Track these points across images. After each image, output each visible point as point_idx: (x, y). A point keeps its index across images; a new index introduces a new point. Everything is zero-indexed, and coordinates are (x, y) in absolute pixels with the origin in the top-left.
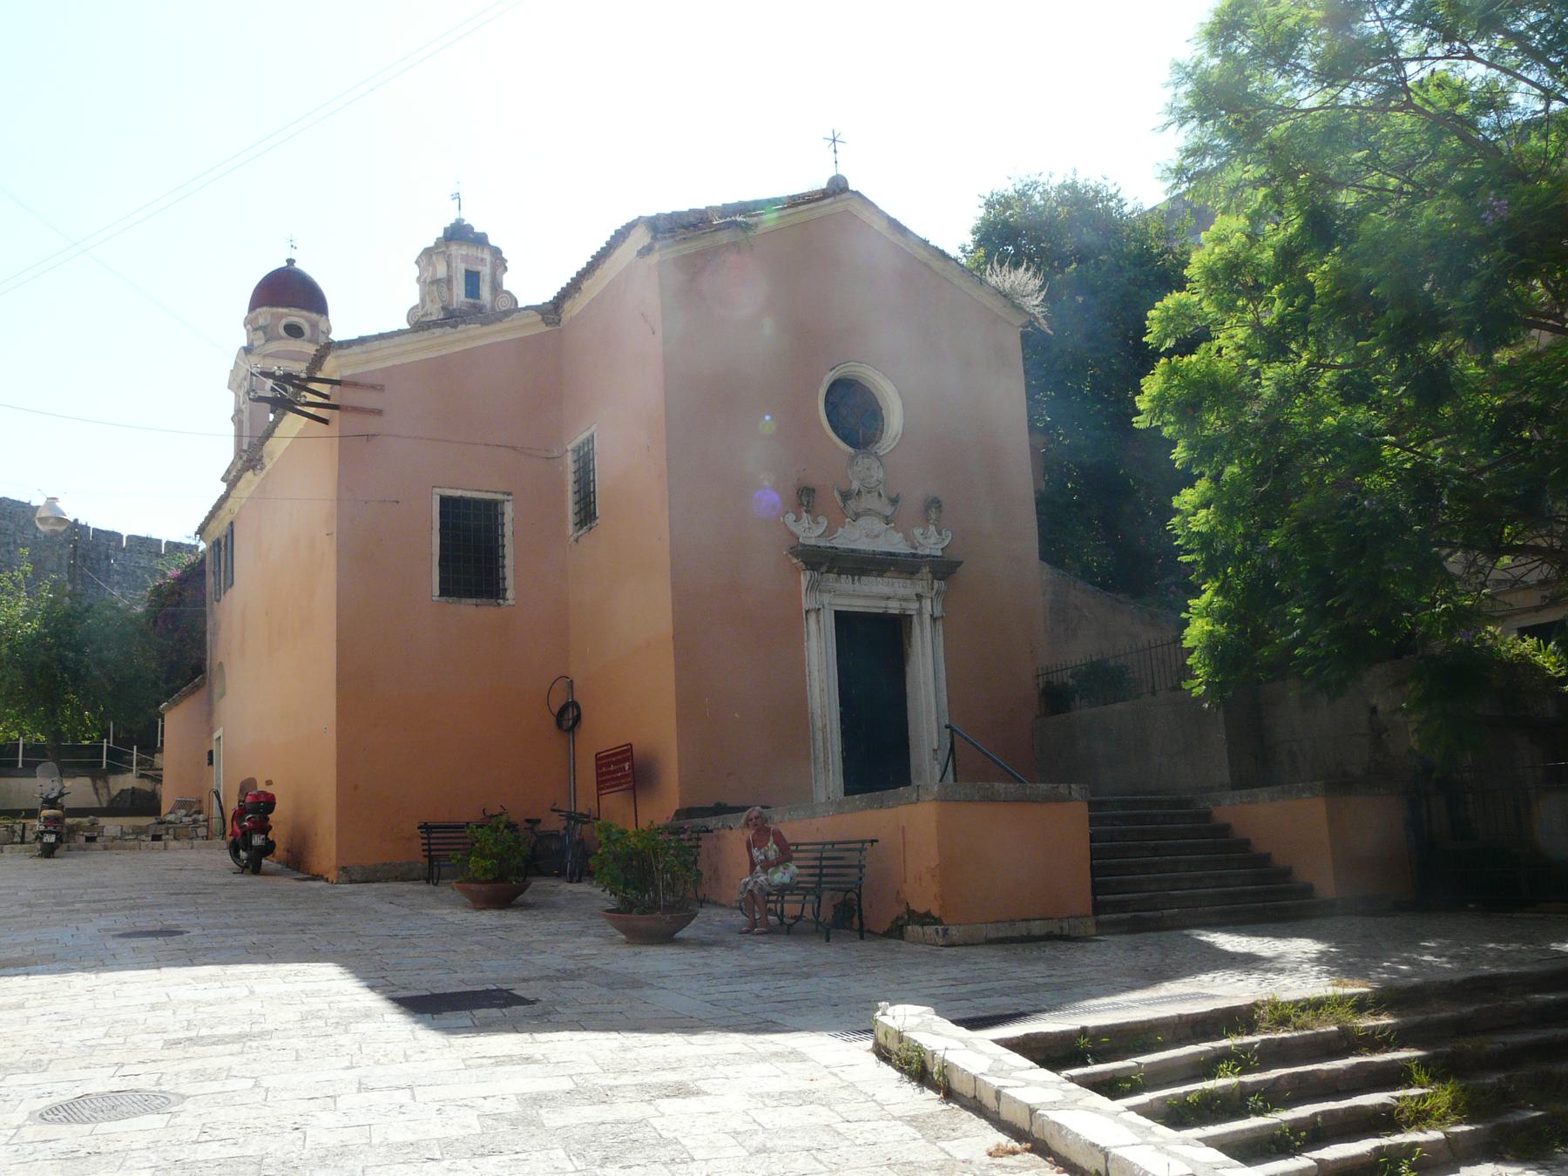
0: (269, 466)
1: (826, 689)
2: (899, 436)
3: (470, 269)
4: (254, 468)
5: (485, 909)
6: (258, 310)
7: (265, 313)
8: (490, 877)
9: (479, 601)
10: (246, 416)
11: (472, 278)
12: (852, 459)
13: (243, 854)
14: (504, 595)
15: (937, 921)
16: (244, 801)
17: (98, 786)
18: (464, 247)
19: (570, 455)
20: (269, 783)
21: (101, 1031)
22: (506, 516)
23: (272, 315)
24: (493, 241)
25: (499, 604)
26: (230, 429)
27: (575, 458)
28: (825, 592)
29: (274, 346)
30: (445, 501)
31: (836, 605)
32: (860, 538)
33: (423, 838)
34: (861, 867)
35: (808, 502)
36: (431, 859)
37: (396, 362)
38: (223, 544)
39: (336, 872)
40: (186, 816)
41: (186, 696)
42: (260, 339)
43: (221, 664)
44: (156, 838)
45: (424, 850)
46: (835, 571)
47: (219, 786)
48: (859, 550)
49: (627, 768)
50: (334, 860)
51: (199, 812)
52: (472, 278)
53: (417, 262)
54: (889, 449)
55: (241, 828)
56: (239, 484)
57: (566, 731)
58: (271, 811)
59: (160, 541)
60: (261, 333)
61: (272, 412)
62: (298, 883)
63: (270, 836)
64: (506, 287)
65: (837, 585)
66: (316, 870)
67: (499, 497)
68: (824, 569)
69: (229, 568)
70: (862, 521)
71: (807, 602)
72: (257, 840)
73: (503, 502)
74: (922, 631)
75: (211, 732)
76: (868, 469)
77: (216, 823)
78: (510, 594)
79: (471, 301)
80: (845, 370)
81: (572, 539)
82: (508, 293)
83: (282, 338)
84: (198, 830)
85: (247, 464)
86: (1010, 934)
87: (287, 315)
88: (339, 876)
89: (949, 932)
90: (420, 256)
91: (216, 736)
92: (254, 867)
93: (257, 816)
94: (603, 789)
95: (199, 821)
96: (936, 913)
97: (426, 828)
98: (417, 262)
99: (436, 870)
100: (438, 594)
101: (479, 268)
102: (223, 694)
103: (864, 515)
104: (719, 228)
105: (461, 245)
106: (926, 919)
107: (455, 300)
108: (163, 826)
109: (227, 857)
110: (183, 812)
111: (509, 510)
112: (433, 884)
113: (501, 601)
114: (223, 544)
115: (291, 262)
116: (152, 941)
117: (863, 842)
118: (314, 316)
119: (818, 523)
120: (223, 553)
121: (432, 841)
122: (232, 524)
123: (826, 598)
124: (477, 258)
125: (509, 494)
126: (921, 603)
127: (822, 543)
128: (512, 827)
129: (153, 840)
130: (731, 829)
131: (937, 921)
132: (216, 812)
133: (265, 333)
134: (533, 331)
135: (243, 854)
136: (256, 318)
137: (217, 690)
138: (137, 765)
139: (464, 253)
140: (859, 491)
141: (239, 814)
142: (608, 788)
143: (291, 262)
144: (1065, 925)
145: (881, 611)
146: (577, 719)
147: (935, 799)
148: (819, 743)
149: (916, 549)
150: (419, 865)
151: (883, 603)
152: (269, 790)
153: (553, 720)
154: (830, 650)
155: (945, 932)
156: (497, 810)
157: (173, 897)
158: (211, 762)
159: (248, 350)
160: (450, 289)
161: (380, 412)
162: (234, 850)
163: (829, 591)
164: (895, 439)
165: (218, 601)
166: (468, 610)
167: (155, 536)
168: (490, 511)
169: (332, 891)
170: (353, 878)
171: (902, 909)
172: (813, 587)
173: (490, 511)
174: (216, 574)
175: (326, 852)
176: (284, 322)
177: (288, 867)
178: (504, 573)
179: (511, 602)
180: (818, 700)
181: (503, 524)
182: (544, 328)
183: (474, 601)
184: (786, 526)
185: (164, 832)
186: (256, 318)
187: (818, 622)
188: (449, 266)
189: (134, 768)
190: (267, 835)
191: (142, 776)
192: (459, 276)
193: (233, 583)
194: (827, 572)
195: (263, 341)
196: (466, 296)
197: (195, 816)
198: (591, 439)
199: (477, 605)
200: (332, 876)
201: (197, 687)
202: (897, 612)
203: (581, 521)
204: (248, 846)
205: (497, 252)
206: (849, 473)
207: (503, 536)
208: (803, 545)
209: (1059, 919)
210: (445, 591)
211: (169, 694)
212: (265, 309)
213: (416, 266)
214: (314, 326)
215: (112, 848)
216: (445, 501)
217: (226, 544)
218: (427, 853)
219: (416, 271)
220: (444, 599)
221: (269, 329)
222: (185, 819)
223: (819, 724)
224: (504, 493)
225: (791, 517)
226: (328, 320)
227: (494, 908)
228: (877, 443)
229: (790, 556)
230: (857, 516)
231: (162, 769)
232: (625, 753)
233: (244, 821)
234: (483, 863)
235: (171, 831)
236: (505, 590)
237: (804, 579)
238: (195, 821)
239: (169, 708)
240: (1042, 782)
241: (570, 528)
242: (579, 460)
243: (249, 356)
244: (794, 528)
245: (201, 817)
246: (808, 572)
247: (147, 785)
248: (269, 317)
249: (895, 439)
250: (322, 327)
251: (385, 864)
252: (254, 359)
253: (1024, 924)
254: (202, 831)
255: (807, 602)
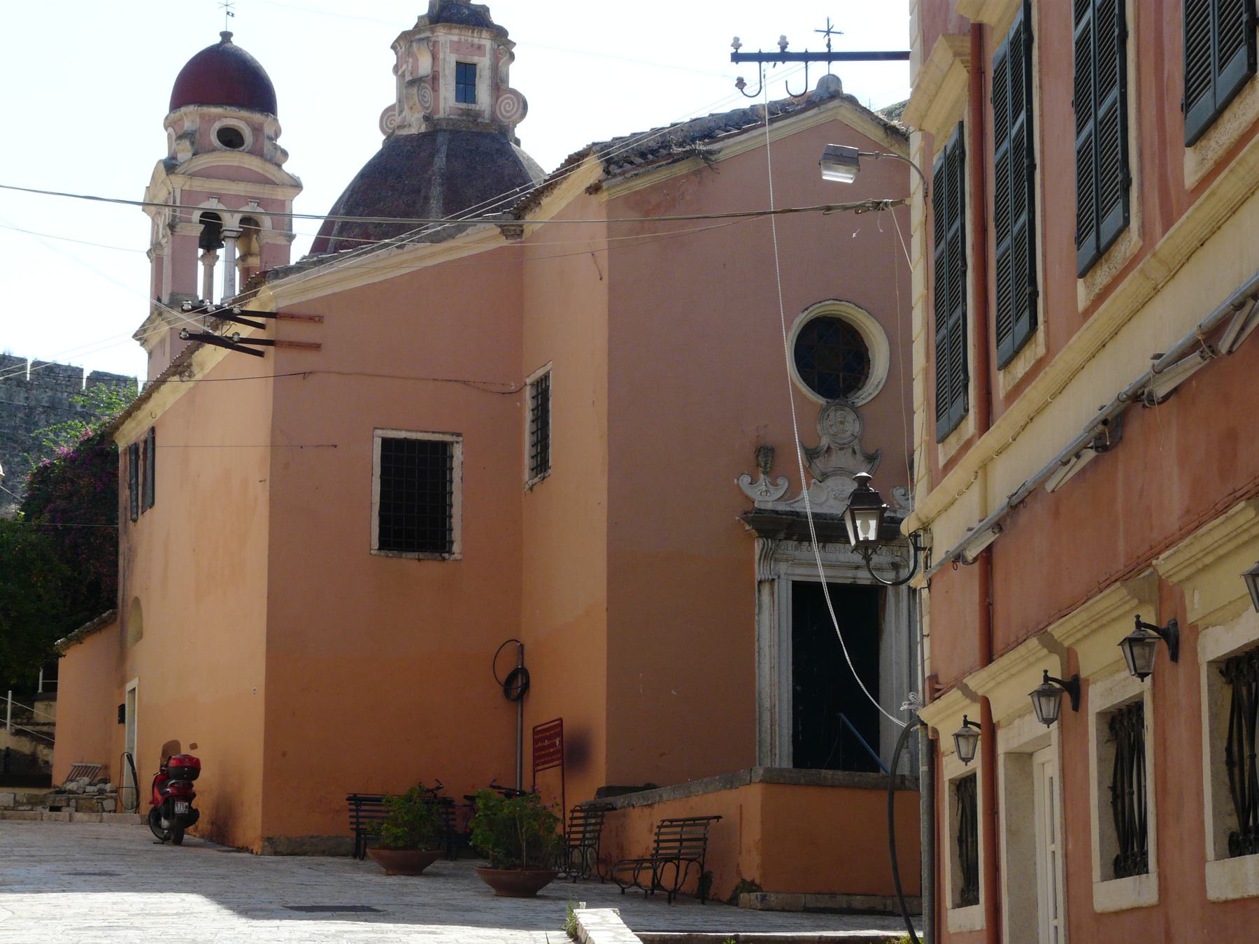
0: (199, 376)
1: (776, 667)
2: (883, 382)
3: (462, 60)
4: (181, 374)
5: (395, 875)
6: (183, 110)
7: (192, 115)
8: (401, 843)
9: (421, 556)
10: (167, 251)
11: (466, 74)
12: (824, 410)
13: (165, 823)
14: (451, 547)
15: (758, 888)
16: (166, 766)
17: (1041, 701)
18: (456, 31)
19: (528, 388)
20: (194, 746)
21: (87, 910)
22: (455, 459)
23: (202, 117)
24: (496, 18)
25: (444, 559)
26: (146, 267)
27: (534, 393)
28: (781, 561)
29: (204, 161)
30: (386, 443)
31: (793, 575)
32: (827, 500)
33: (351, 810)
34: (705, 840)
35: (766, 464)
36: (359, 832)
37: (337, 289)
38: (141, 450)
39: (261, 843)
40: (90, 784)
41: (89, 632)
42: (185, 154)
43: (137, 600)
44: (54, 809)
45: (351, 823)
46: (795, 537)
47: (133, 749)
48: (826, 514)
49: (558, 743)
50: (260, 830)
51: (105, 781)
52: (466, 74)
53: (393, 47)
54: (871, 398)
55: (162, 794)
56: (163, 387)
57: (513, 700)
58: (196, 776)
59: (24, 360)
60: (186, 144)
61: (201, 246)
62: (219, 853)
63: (194, 805)
64: (513, 84)
65: (797, 553)
66: (240, 843)
67: (448, 438)
68: (782, 535)
69: (149, 479)
70: (830, 482)
71: (760, 572)
72: (180, 808)
73: (452, 443)
74: (897, 602)
75: (123, 681)
76: (842, 423)
77: (127, 794)
78: (456, 548)
79: (463, 106)
80: (822, 309)
81: (527, 487)
82: (514, 92)
83: (214, 150)
84: (105, 803)
85: (173, 369)
86: (829, 905)
87: (220, 117)
88: (263, 847)
89: (767, 898)
90: (397, 41)
91: (129, 687)
92: (175, 837)
93: (181, 782)
94: (538, 765)
95: (106, 791)
96: (757, 881)
97: (356, 800)
98: (393, 47)
99: (363, 842)
100: (377, 547)
101: (475, 59)
102: (140, 635)
103: (832, 475)
104: (676, 160)
105: (450, 28)
106: (751, 887)
107: (442, 105)
108: (64, 797)
109: (147, 832)
110: (86, 780)
111: (458, 452)
112: (360, 859)
113: (446, 555)
114: (141, 450)
115: (226, 36)
116: (98, 878)
117: (709, 819)
118: (257, 117)
119: (777, 485)
120: (141, 462)
121: (361, 814)
122: (153, 430)
123: (783, 568)
124: (472, 45)
125: (459, 435)
126: (897, 573)
127: (782, 507)
128: (448, 803)
129: (50, 811)
130: (634, 807)
131: (758, 888)
132: (127, 780)
133: (192, 143)
134: (493, 245)
135: (165, 823)
136: (181, 119)
137: (131, 631)
138: (12, 718)
139: (455, 38)
140: (829, 448)
141: (160, 782)
142: (543, 764)
143: (226, 36)
144: (889, 902)
145: (849, 581)
146: (526, 686)
147: (761, 781)
148: (767, 724)
149: (895, 512)
150: (348, 840)
151: (850, 573)
152: (194, 754)
153: (499, 690)
154: (784, 624)
155: (764, 898)
156: (432, 785)
157: (101, 856)
158: (122, 720)
159: (170, 166)
160: (435, 89)
161: (316, 347)
162: (153, 820)
163: (787, 561)
164: (877, 386)
165: (135, 521)
166: (410, 565)
167: (17, 353)
168: (437, 453)
169: (255, 860)
170: (279, 849)
171: (737, 880)
172: (767, 556)
173: (437, 453)
174: (133, 487)
175: (251, 824)
176: (217, 125)
177: (211, 840)
178: (450, 523)
179: (457, 556)
180: (768, 677)
181: (451, 469)
182: (504, 242)
183: (415, 555)
184: (740, 489)
185: (64, 804)
186: (181, 119)
187: (772, 594)
188: (434, 57)
189: (8, 721)
190: (190, 804)
191: (18, 733)
192: (447, 72)
193: (153, 503)
194: (786, 539)
195: (190, 154)
196: (457, 100)
197: (101, 786)
198: (546, 378)
199: (419, 560)
200: (257, 847)
201: (104, 624)
202: (868, 582)
203: (537, 467)
204: (170, 814)
205: (500, 34)
206: (819, 427)
207: (451, 482)
208: (760, 511)
209: (884, 897)
210: (384, 544)
211: (66, 631)
212: (191, 108)
213: (392, 52)
214: (257, 130)
215: (9, 818)
216: (386, 443)
217: (145, 450)
218: (354, 826)
219: (392, 58)
220: (383, 553)
221: (197, 135)
222: (89, 789)
223: (767, 704)
224: (453, 434)
225: (746, 479)
226: (276, 120)
227: (401, 874)
228: (859, 389)
229: (742, 522)
230: (824, 476)
231: (54, 724)
232: (557, 727)
233: (166, 787)
234: (395, 830)
235: (73, 803)
236: (452, 542)
237: (758, 546)
238: (101, 792)
239: (67, 646)
240: (870, 772)
241: (526, 474)
242: (537, 396)
243: (172, 177)
244: (749, 492)
245: (108, 787)
246: (761, 541)
247: (25, 746)
248: (198, 120)
249: (877, 386)
250: (268, 130)
251: (312, 837)
252: (178, 182)
253: (845, 898)
254: (109, 804)
255: (760, 572)
